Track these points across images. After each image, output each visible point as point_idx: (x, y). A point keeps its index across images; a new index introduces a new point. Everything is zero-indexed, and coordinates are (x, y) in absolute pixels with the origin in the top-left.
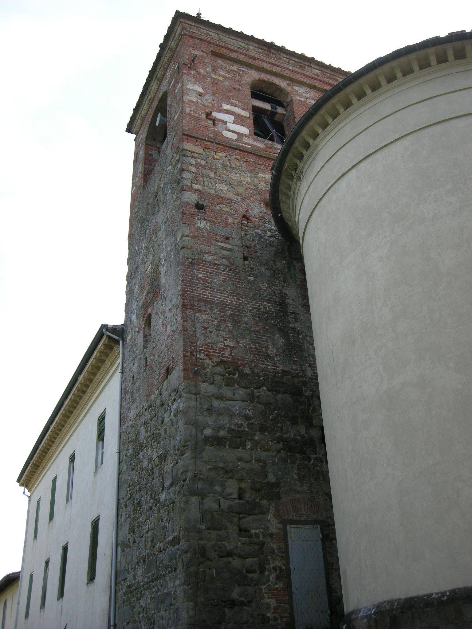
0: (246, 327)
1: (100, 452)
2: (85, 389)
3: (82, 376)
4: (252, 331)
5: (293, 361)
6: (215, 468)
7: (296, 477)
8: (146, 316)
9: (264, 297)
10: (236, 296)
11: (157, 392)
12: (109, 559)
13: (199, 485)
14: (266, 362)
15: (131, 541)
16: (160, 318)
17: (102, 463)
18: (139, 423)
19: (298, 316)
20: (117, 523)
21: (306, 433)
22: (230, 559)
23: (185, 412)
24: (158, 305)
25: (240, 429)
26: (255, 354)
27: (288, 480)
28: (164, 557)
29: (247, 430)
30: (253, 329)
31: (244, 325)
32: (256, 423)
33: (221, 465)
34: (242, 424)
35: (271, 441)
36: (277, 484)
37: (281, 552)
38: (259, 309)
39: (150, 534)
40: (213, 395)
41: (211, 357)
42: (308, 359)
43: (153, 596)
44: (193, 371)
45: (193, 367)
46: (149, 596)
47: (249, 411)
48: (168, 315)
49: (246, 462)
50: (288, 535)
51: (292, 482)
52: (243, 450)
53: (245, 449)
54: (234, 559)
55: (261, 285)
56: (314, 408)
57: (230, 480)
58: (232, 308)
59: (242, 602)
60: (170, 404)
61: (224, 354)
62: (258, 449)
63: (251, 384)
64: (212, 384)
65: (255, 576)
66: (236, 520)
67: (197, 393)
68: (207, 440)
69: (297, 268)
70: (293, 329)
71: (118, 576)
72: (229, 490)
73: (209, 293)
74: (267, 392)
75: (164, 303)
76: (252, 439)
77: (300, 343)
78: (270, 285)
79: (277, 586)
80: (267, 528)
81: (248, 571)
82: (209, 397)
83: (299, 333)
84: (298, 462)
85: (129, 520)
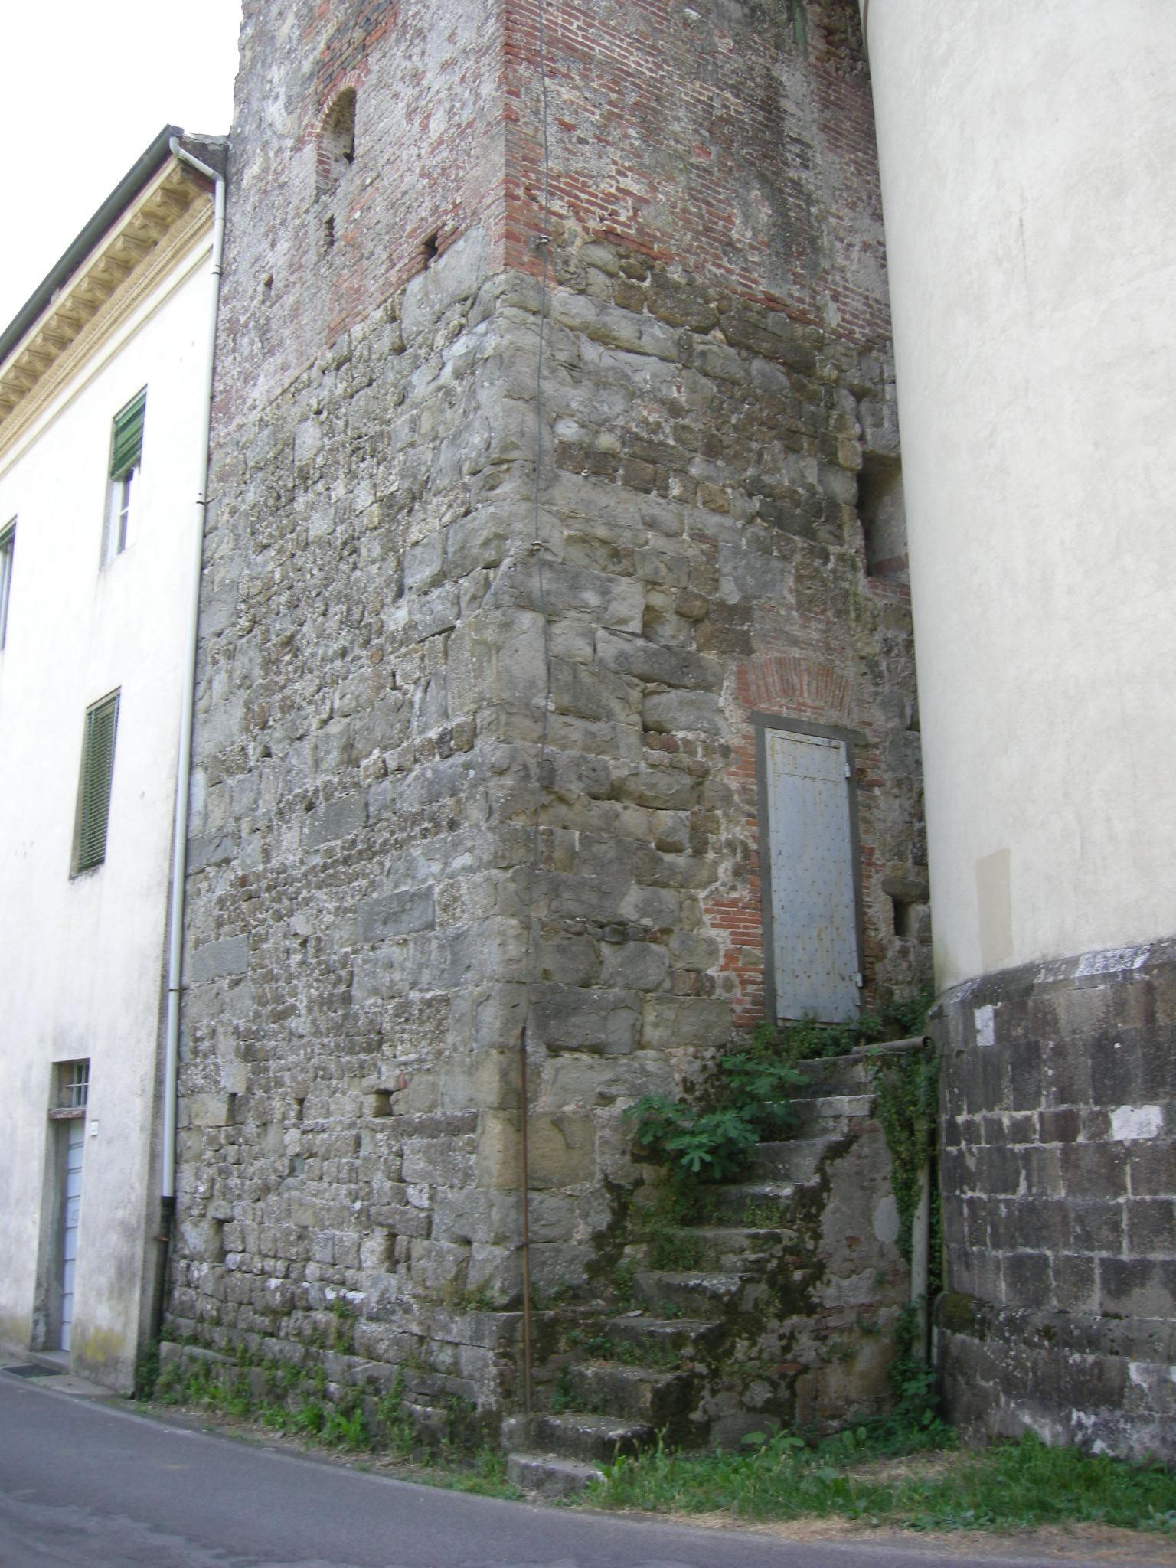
0: (676, 151)
1: (117, 512)
2: (68, 332)
3: (68, 290)
4: (692, 165)
5: (794, 274)
6: (584, 540)
7: (791, 599)
8: (333, 98)
9: (724, 75)
10: (652, 55)
11: (378, 315)
12: (166, 808)
13: (539, 582)
14: (725, 262)
15: (250, 751)
16: (396, 95)
17: (122, 546)
18: (296, 411)
19: (810, 153)
20: (194, 703)
21: (820, 481)
22: (618, 806)
23: (503, 360)
24: (391, 58)
25: (653, 437)
26: (697, 232)
27: (772, 603)
28: (410, 793)
29: (671, 442)
30: (693, 160)
31: (672, 143)
32: (696, 426)
33: (602, 532)
34: (658, 425)
35: (733, 487)
36: (742, 611)
37: (749, 802)
38: (712, 107)
39: (335, 727)
40: (584, 328)
41: (582, 214)
42: (830, 278)
43: (349, 902)
44: (533, 246)
45: (532, 233)
46: (332, 906)
47: (679, 391)
48: (435, 81)
49: (668, 535)
50: (768, 758)
51: (782, 612)
52: (659, 500)
53: (665, 497)
54: (625, 808)
55: (717, 39)
56: (841, 417)
57: (625, 580)
58: (640, 88)
59: (646, 930)
60: (439, 341)
61: (614, 213)
62: (699, 504)
63: (687, 315)
64: (581, 292)
65: (680, 860)
66: (635, 695)
67: (542, 312)
68: (565, 450)
69: (809, 16)
70: (796, 184)
71: (195, 855)
72: (619, 608)
73: (579, 28)
74: (725, 347)
75: (416, 50)
76: (683, 472)
77: (811, 227)
78: (741, 45)
79: (735, 895)
80: (715, 732)
81: (665, 847)
82: (572, 329)
83: (810, 201)
84: (798, 558)
85: (244, 694)
